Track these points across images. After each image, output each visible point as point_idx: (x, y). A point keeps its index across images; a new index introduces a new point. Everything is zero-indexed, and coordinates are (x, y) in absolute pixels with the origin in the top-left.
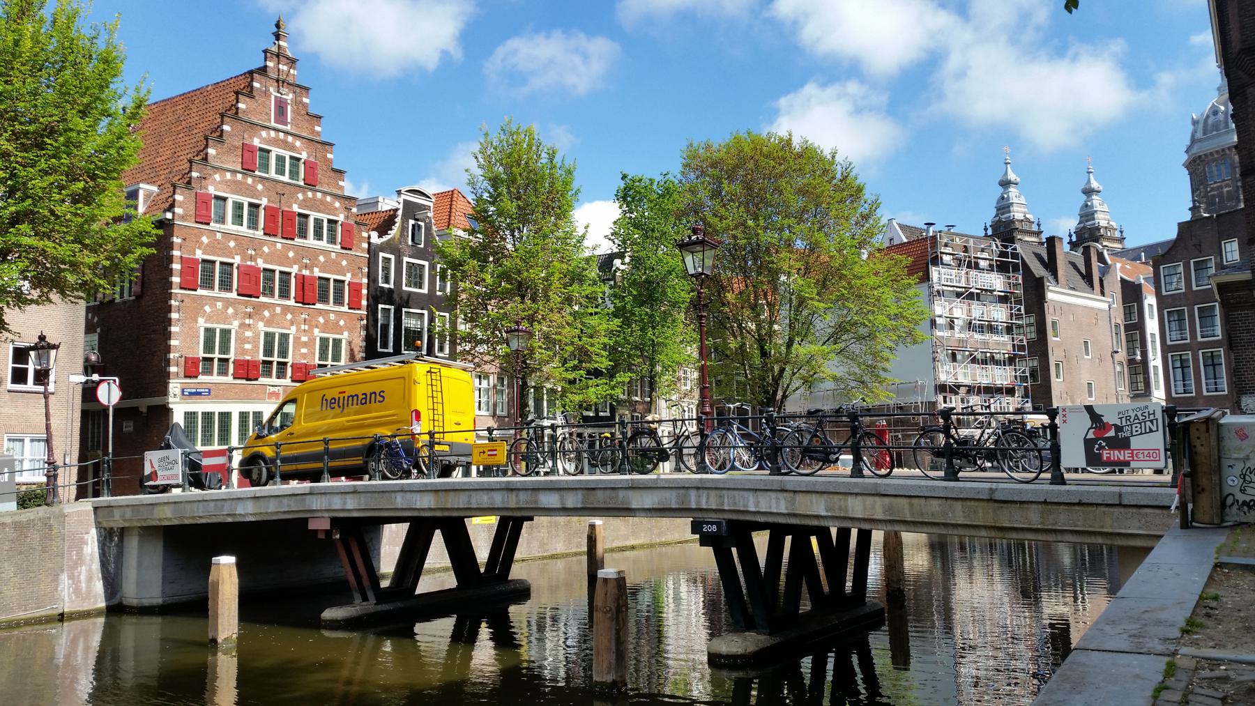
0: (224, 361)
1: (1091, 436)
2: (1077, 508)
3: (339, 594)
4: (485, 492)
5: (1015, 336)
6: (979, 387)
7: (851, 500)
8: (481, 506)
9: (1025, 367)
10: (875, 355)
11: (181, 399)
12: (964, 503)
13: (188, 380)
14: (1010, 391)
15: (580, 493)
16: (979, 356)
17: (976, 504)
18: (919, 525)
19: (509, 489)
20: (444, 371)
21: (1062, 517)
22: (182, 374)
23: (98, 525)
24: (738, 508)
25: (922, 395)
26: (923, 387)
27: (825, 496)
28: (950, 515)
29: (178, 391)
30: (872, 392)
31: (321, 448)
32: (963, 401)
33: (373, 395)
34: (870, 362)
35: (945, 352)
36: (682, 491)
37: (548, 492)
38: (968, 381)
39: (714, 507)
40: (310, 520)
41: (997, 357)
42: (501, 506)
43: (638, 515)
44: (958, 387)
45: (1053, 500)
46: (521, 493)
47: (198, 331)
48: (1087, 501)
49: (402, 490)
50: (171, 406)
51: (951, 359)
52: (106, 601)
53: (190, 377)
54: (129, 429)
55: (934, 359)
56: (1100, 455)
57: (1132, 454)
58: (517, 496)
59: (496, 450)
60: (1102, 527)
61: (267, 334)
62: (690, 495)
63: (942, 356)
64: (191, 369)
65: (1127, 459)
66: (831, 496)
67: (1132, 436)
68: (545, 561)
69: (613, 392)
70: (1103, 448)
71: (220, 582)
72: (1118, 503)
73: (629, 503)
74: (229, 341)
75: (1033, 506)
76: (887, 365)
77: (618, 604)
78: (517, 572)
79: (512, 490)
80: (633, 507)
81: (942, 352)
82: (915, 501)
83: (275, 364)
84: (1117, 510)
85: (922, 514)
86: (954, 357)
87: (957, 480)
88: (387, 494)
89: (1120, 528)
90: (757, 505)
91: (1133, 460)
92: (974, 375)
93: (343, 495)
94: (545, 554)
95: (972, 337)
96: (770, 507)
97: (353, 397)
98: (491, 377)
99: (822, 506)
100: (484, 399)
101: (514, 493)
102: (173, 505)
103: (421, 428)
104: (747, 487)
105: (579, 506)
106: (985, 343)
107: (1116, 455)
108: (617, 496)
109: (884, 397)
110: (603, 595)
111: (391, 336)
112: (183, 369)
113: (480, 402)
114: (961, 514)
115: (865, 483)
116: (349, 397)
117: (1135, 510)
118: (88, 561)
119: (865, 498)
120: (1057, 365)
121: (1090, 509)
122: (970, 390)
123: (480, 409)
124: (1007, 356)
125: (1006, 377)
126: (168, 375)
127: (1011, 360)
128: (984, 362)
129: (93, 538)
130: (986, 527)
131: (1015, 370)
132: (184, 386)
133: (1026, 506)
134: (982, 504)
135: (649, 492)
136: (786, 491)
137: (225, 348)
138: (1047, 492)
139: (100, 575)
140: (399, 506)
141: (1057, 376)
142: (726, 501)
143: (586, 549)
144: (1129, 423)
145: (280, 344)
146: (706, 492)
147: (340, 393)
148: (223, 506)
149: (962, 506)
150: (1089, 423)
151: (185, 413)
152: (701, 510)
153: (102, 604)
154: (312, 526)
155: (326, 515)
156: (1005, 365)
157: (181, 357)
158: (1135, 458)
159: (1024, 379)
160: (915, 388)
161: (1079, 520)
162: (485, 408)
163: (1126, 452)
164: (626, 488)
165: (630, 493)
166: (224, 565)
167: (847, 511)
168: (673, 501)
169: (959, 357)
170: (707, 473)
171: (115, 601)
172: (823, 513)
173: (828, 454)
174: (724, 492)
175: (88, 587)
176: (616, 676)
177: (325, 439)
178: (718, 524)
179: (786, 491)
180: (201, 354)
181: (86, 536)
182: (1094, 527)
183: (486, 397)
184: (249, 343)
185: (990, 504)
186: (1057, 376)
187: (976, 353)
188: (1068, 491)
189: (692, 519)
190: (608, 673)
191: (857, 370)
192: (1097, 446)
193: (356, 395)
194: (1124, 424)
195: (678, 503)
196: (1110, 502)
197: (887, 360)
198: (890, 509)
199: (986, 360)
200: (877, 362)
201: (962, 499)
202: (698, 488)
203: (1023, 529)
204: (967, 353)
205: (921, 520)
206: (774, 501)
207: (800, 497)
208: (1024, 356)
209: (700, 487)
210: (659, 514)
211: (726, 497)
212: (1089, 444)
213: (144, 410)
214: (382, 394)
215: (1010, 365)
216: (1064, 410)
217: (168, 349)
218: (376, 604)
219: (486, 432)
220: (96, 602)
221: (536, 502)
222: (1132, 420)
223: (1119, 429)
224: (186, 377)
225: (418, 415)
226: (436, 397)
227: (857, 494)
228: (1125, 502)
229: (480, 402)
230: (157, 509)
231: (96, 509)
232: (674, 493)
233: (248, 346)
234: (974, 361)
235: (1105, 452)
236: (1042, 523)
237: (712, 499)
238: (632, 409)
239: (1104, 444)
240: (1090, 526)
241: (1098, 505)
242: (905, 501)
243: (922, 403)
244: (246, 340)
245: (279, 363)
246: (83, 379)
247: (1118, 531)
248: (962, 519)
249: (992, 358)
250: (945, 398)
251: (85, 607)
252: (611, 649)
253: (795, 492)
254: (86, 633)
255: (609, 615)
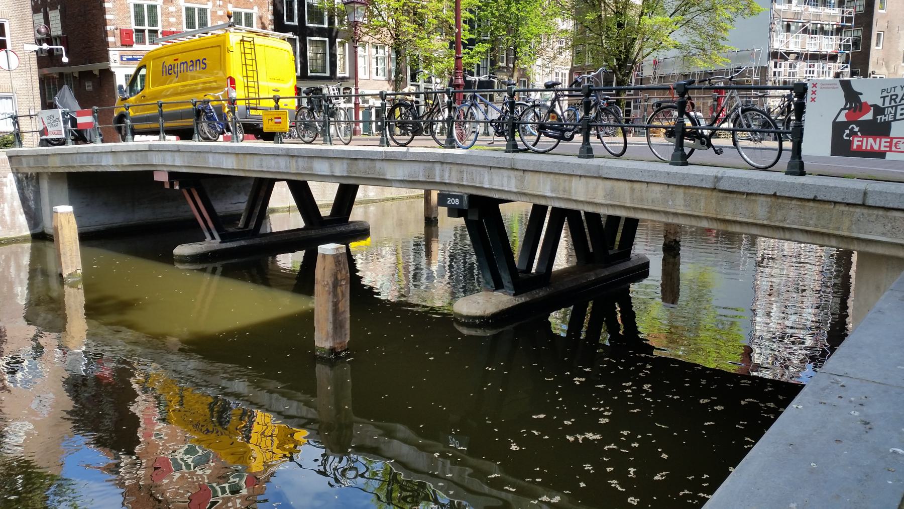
0: (154, 32)
1: (842, 118)
2: (811, 204)
3: (191, 231)
4: (273, 157)
5: (845, 9)
6: (806, 55)
7: (575, 182)
8: (271, 170)
9: (849, 38)
10: (715, 25)
11: (121, 64)
12: (687, 191)
13: (125, 48)
14: (833, 58)
15: (345, 161)
16: (810, 27)
17: (700, 192)
18: (640, 211)
19: (291, 155)
20: (258, 40)
21: (793, 213)
22: (119, 43)
23: (16, 173)
24: (474, 185)
25: (756, 62)
26: (758, 54)
27: (552, 176)
28: (670, 203)
29: (118, 58)
30: (710, 58)
31: (156, 112)
32: (790, 67)
33: (198, 62)
34: (711, 32)
35: (781, 23)
36: (428, 165)
37: (320, 160)
38: (797, 49)
39: (455, 182)
40: (154, 173)
41: (826, 28)
42: (284, 171)
43: (394, 185)
44: (788, 54)
45: (783, 194)
46: (300, 159)
47: (128, 7)
48: (824, 198)
49: (211, 151)
50: (113, 70)
51: (785, 29)
52: (30, 230)
53: (126, 46)
54: (89, 88)
55: (771, 30)
56: (850, 143)
57: (891, 143)
58: (297, 162)
59: (280, 118)
60: (838, 229)
61: (187, 9)
62: (435, 169)
63: (778, 27)
64: (126, 39)
65: (882, 148)
66: (557, 177)
67: (895, 120)
68: (412, 200)
69: (471, 61)
70: (855, 134)
71: (59, 228)
72: (860, 203)
73: (384, 174)
74: (156, 14)
75: (762, 199)
76: (725, 35)
77: (336, 279)
78: (357, 214)
79: (293, 156)
80: (388, 178)
81: (778, 23)
82: (637, 186)
83: (147, 32)
84: (858, 210)
85: (642, 200)
86: (788, 28)
87: (687, 164)
88: (202, 154)
89: (859, 233)
90: (491, 182)
91: (890, 151)
92: (803, 44)
93: (173, 154)
94: (412, 194)
95: (806, 10)
96: (502, 185)
97: (183, 63)
98: (387, 47)
99: (548, 187)
100: (380, 67)
101: (295, 159)
102: (60, 156)
103: (238, 93)
104: (482, 164)
105: (345, 174)
106: (817, 16)
107: (870, 143)
108: (375, 167)
109: (720, 62)
110: (322, 269)
111: (296, 12)
112: (119, 39)
113: (377, 69)
114: (683, 201)
115: (589, 166)
116: (181, 64)
117: (881, 212)
118: (9, 197)
119: (589, 180)
120: (879, 35)
121: (827, 206)
122: (799, 56)
123: (377, 75)
124: (835, 27)
125: (832, 46)
126: (107, 44)
127: (839, 31)
128: (815, 32)
129: (11, 181)
130: (707, 218)
131: (841, 39)
132: (122, 53)
133: (753, 198)
134: (705, 193)
135: (401, 163)
136: (517, 170)
137: (153, 21)
138: (779, 184)
139: (22, 210)
140: (212, 166)
141: (877, 45)
142: (465, 176)
143: (274, 230)
144: (893, 104)
145: (200, 17)
146: (448, 166)
147: (175, 60)
148: (92, 158)
149: (685, 193)
150: (842, 102)
151: (126, 76)
152: (445, 184)
153: (27, 232)
154: (158, 177)
155: (165, 169)
156: (832, 35)
157: (117, 29)
158: (894, 149)
159: (847, 47)
160: (752, 55)
161: (811, 219)
162: (382, 74)
163: (883, 140)
164: (382, 160)
165: (386, 165)
166: (62, 213)
167: (570, 193)
168: (421, 174)
169: (793, 28)
170: (453, 147)
171: (38, 230)
172: (549, 194)
173: (563, 131)
174: (464, 168)
175: (13, 220)
176: (334, 343)
177: (274, 96)
178: (460, 197)
179: (517, 170)
180: (133, 27)
181: (4, 180)
182: (828, 228)
183: (383, 64)
184: (173, 16)
185: (715, 193)
186: (877, 45)
187: (808, 25)
188: (803, 185)
189: (439, 192)
190: (327, 340)
191: (698, 39)
192: (847, 132)
193: (186, 62)
194: (887, 104)
195: (425, 177)
196: (851, 201)
197: (726, 30)
198: (611, 193)
199: (816, 31)
200: (717, 31)
201: (685, 187)
202: (442, 163)
203: (747, 224)
204: (800, 24)
205: (640, 206)
206: (505, 179)
207: (528, 176)
208: (850, 27)
209: (443, 161)
210: (411, 185)
211: (465, 173)
212: (838, 128)
213: (96, 73)
214: (204, 61)
215: (837, 34)
216: (814, 85)
217: (104, 22)
218: (220, 243)
219: (272, 101)
220: (20, 231)
221: (311, 168)
222: (898, 100)
223: (879, 110)
224: (123, 45)
225: (232, 81)
226: (250, 64)
227: (580, 176)
228: (870, 202)
229: (377, 69)
230: (51, 159)
231: (10, 157)
232: (422, 166)
233: (172, 20)
234: (805, 31)
235: (856, 139)
236: (769, 219)
237: (454, 174)
238: (509, 74)
239: (856, 129)
240: (824, 227)
241: (835, 203)
242: (627, 185)
243: (755, 68)
244: (169, 15)
245: (150, 31)
246: (37, 47)
247: (855, 235)
248: (682, 208)
249: (822, 28)
250: (776, 64)
251: (12, 235)
252: (328, 319)
253: (524, 171)
254: (17, 255)
255: (327, 289)
